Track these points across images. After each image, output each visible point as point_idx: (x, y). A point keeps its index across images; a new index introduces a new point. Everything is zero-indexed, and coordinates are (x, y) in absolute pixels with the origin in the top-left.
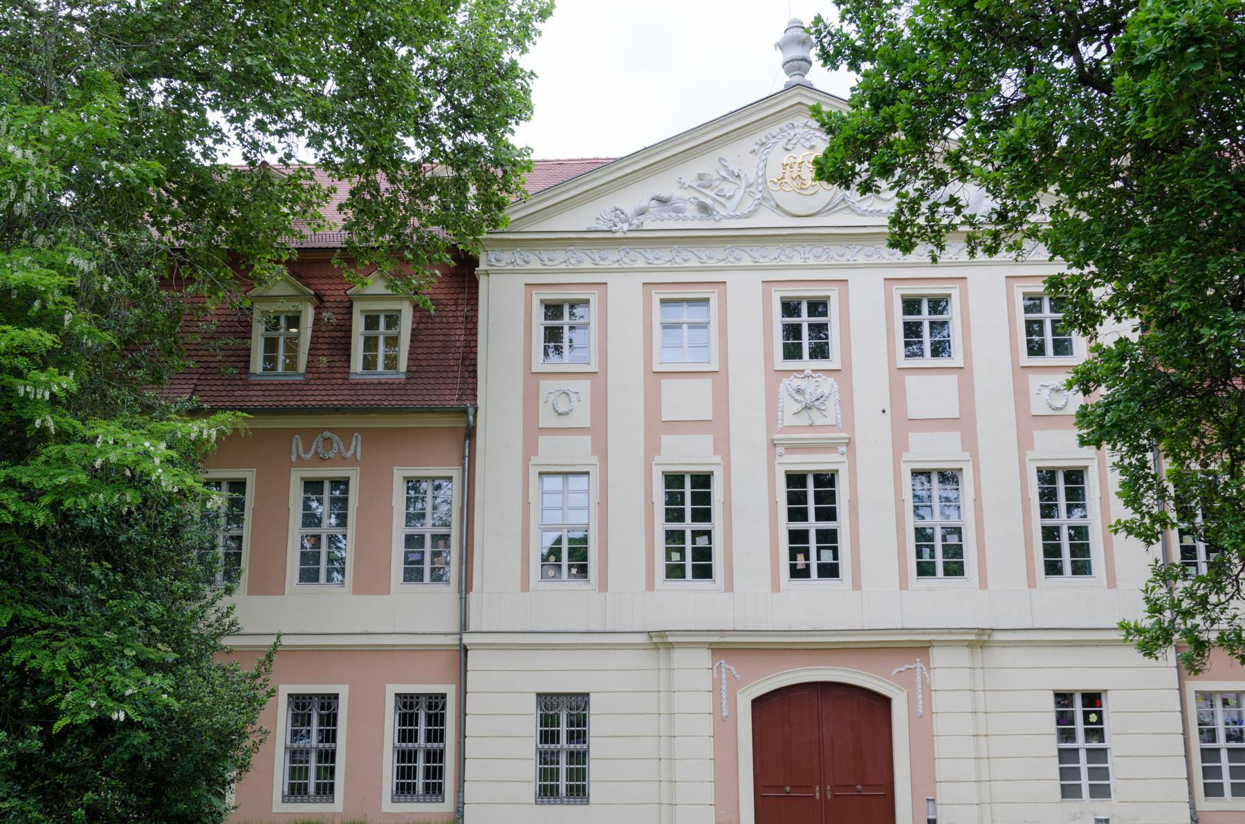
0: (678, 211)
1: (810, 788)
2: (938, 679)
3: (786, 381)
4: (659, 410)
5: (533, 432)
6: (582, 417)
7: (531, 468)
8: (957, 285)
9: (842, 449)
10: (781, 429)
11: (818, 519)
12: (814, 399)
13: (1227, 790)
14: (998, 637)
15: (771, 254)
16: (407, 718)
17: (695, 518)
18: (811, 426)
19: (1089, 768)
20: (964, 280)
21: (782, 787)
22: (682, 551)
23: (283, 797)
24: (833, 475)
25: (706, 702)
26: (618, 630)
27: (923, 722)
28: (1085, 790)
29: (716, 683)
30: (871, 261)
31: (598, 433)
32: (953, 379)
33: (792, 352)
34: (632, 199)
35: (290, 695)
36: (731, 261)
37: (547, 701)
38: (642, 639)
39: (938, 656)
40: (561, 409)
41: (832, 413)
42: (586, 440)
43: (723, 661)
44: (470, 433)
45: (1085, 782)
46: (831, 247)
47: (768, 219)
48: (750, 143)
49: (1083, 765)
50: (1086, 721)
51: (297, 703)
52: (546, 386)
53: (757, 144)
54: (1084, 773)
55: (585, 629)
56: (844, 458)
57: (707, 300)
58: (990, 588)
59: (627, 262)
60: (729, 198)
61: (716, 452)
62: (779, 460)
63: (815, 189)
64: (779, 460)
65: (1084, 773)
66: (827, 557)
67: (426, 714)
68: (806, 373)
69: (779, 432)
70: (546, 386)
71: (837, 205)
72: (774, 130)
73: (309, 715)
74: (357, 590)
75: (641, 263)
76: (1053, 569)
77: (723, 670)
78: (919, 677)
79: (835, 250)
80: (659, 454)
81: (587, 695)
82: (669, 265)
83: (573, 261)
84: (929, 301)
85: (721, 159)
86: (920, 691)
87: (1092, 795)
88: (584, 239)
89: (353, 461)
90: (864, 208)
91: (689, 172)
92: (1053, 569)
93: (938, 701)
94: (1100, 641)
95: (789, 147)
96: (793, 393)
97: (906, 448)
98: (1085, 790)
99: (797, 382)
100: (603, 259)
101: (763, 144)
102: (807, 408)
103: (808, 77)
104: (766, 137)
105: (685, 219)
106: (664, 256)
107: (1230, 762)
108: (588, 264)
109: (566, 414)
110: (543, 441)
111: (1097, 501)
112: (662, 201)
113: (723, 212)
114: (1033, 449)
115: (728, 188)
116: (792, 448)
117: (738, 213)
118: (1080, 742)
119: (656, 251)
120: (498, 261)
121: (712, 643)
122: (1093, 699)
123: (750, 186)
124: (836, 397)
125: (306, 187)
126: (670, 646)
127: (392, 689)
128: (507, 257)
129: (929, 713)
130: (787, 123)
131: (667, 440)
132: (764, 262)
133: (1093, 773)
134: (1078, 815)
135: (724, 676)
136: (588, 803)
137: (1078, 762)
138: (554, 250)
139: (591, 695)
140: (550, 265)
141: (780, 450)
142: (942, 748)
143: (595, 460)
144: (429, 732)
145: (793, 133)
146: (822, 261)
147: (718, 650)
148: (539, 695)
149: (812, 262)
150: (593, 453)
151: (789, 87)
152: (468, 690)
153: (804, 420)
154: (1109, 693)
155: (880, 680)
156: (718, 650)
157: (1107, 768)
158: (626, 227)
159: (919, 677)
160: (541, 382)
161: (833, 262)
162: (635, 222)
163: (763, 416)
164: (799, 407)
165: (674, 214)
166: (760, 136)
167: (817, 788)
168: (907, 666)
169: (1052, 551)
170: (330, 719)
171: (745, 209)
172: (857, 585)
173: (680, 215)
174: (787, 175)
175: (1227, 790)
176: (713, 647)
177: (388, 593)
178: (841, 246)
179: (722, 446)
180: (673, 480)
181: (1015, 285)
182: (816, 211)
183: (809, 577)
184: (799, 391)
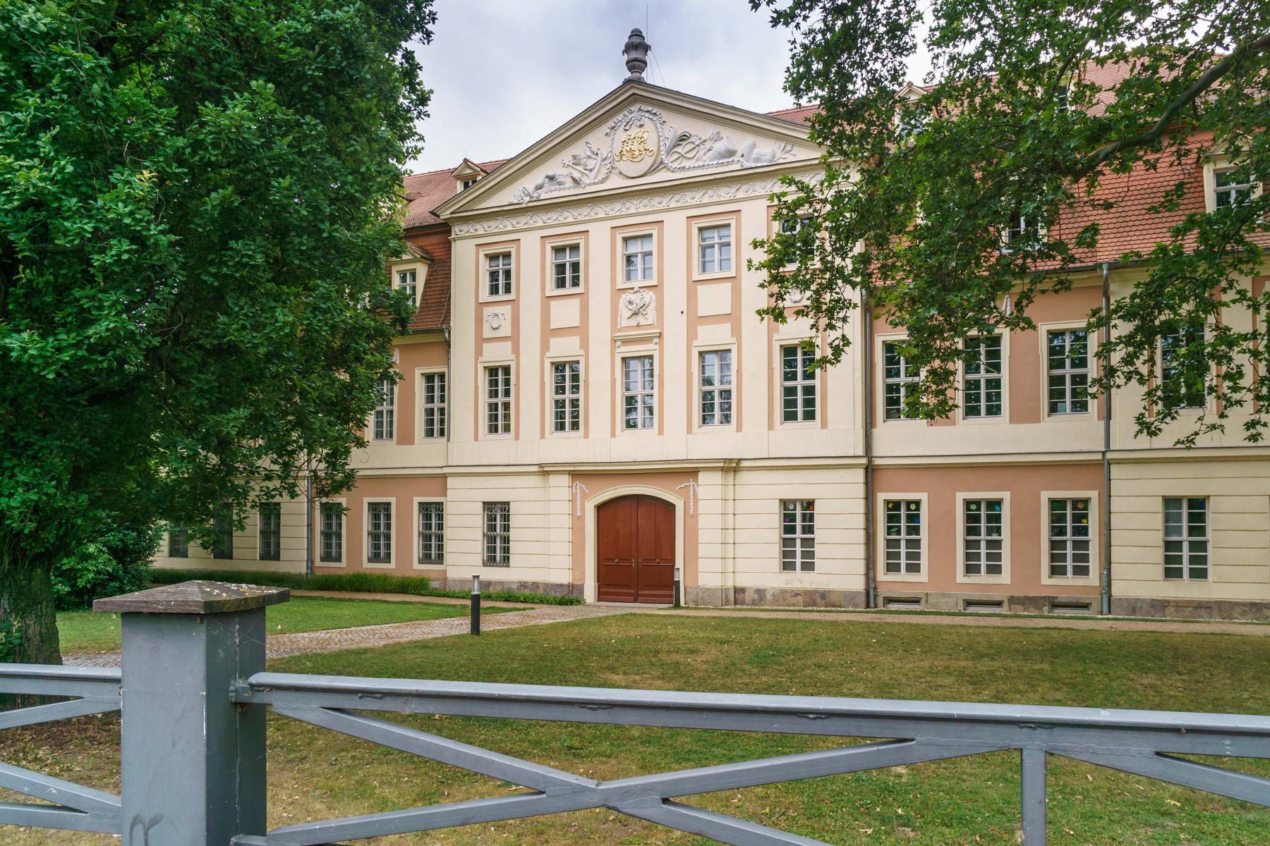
1: (629, 560)
2: (702, 492)
3: (623, 296)
5: (480, 340)
6: (506, 331)
7: (479, 365)
8: (734, 216)
9: (656, 340)
13: (903, 567)
14: (744, 464)
15: (616, 208)
16: (972, 518)
17: (1074, 365)
21: (614, 560)
27: (692, 518)
28: (798, 566)
29: (574, 495)
30: (679, 205)
31: (514, 339)
35: (420, 503)
36: (592, 215)
37: (489, 506)
38: (535, 469)
41: (650, 316)
42: (508, 345)
44: (448, 344)
47: (616, 182)
48: (605, 129)
52: (488, 311)
57: (650, 236)
59: (532, 224)
60: (591, 170)
61: (581, 348)
62: (618, 350)
64: (618, 350)
72: (620, 117)
74: (399, 443)
76: (790, 416)
79: (493, 224)
81: (508, 503)
87: (1075, 573)
92: (790, 416)
93: (702, 507)
97: (696, 337)
98: (798, 566)
102: (636, 314)
103: (643, 75)
106: (553, 217)
109: (497, 328)
110: (486, 346)
112: (551, 178)
115: (591, 164)
116: (626, 342)
118: (799, 535)
123: (605, 159)
124: (653, 305)
126: (548, 473)
127: (417, 500)
128: (465, 228)
131: (554, 342)
133: (804, 555)
141: (619, 343)
144: (804, 527)
147: (576, 475)
148: (484, 503)
151: (627, 82)
153: (633, 322)
156: (576, 475)
158: (527, 199)
162: (535, 195)
163: (609, 320)
164: (630, 313)
166: (611, 123)
169: (789, 403)
170: (914, 518)
180: (559, 367)
184: (630, 303)
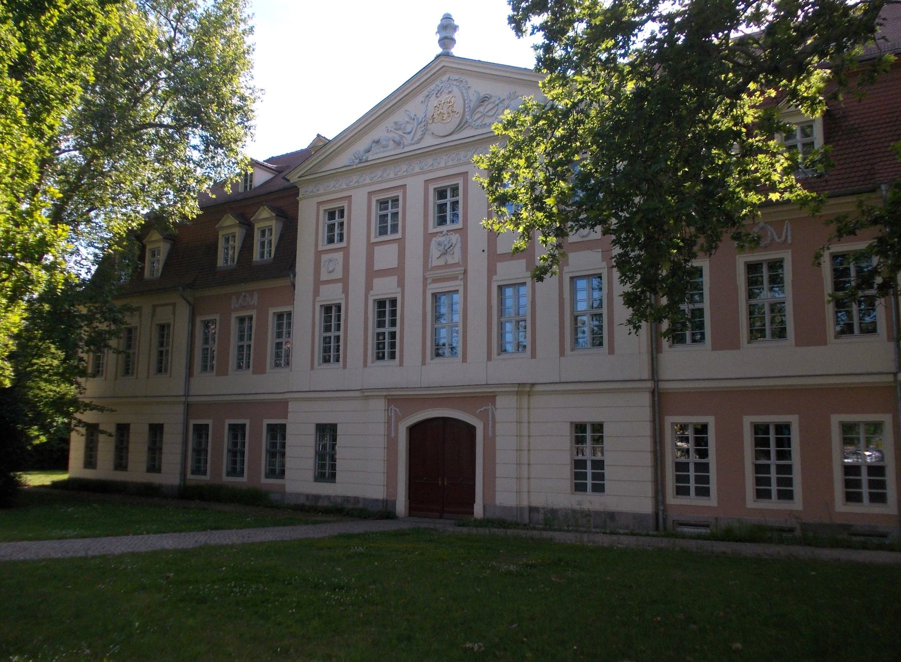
4: (373, 265)
6: (339, 275)
11: (384, 327)
13: (692, 491)
16: (761, 442)
25: (381, 429)
26: (339, 389)
29: (389, 418)
31: (345, 281)
32: (395, 247)
34: (361, 146)
38: (358, 394)
42: (340, 285)
45: (692, 485)
47: (429, 141)
48: (421, 97)
49: (773, 475)
52: (324, 257)
60: (409, 133)
64: (429, 287)
70: (324, 257)
72: (433, 87)
74: (254, 372)
80: (568, 265)
85: (406, 111)
89: (784, 245)
91: (389, 123)
97: (495, 273)
99: (440, 239)
108: (344, 186)
109: (331, 272)
112: (377, 142)
116: (435, 281)
121: (386, 396)
122: (598, 428)
124: (459, 245)
125: (12, 222)
131: (377, 282)
133: (780, 482)
147: (391, 400)
149: (450, 163)
150: (603, 261)
152: (497, 420)
160: (376, 248)
165: (382, 149)
166: (425, 93)
170: (784, 443)
172: (611, 351)
175: (692, 491)
177: (265, 373)
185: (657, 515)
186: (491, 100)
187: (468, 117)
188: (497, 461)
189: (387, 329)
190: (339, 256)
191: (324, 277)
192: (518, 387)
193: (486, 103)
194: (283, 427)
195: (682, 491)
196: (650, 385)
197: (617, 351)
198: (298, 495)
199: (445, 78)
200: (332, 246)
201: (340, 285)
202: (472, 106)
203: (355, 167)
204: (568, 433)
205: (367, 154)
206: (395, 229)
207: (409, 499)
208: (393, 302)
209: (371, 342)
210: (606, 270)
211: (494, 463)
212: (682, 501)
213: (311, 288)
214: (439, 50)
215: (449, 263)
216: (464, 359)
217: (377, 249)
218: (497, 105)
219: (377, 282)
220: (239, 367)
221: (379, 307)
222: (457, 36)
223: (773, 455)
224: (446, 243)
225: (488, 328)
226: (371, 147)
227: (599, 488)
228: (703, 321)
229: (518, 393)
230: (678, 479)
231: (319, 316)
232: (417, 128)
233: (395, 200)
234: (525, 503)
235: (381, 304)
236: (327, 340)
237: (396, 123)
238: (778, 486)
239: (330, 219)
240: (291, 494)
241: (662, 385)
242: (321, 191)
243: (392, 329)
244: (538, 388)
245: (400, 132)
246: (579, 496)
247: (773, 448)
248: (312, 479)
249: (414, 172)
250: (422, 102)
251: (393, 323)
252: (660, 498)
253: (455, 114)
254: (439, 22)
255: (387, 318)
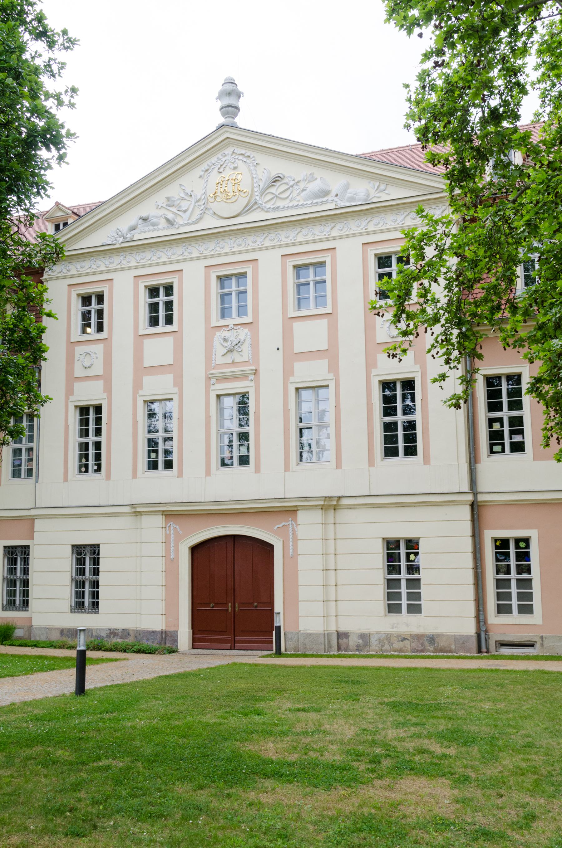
0: (154, 225)
1: (226, 604)
2: (301, 531)
3: (218, 334)
6: (98, 369)
7: (70, 403)
9: (252, 377)
10: (215, 366)
12: (233, 345)
13: (515, 609)
14: (344, 502)
15: (210, 247)
17: (510, 408)
18: (233, 363)
19: (408, 593)
20: (181, 272)
22: (156, 452)
23: (3, 607)
24: (383, 383)
25: (160, 549)
26: (115, 504)
28: (404, 608)
29: (167, 536)
30: (273, 243)
33: (154, 322)
38: (127, 509)
39: (301, 516)
40: (87, 364)
41: (246, 353)
43: (172, 523)
46: (248, 237)
47: (209, 222)
48: (199, 171)
49: (514, 590)
50: (408, 560)
51: (9, 551)
52: (79, 350)
53: (202, 171)
54: (404, 596)
55: (61, 506)
56: (252, 384)
58: (343, 468)
59: (125, 264)
60: (185, 211)
63: (236, 198)
64: (212, 388)
65: (404, 596)
66: (244, 451)
67: (76, 557)
68: (230, 327)
69: (213, 369)
71: (252, 207)
72: (214, 160)
73: (84, 558)
75: (133, 263)
76: (391, 452)
77: (172, 528)
78: (291, 531)
80: (72, 394)
81: (98, 546)
82: (149, 262)
83: (94, 266)
84: (95, 296)
85: (180, 185)
86: (291, 540)
87: (409, 611)
88: (98, 251)
90: (268, 207)
91: (160, 198)
94: (415, 503)
95: (221, 170)
96: (222, 342)
97: (292, 374)
98: (404, 608)
99: (225, 334)
100: (111, 263)
101: (207, 170)
103: (236, 120)
104: (208, 165)
105: (158, 230)
106: (147, 256)
107: (518, 588)
108: (103, 268)
109: (89, 367)
111: (420, 401)
112: (145, 220)
113: (181, 222)
114: (377, 368)
115: (184, 205)
116: (220, 379)
117: (190, 221)
119: (142, 254)
120: (82, 268)
121: (163, 511)
123: (199, 201)
124: (248, 342)
129: (295, 554)
130: (221, 153)
131: (147, 380)
132: (206, 253)
133: (520, 596)
134: (395, 625)
135: (172, 532)
136: (98, 613)
137: (510, 588)
138: (83, 261)
139: (101, 545)
140: (82, 271)
141: (213, 381)
142: (302, 579)
143: (331, 376)
145: (224, 159)
146: (242, 248)
147: (169, 515)
148: (73, 546)
149: (235, 249)
150: (329, 372)
154: (421, 539)
155: (265, 533)
156: (169, 515)
157: (420, 593)
158: (121, 240)
159: (291, 531)
161: (249, 248)
162: (129, 236)
165: (151, 228)
166: (205, 166)
167: (230, 605)
168: (284, 523)
170: (524, 556)
171: (194, 218)
172: (427, 461)
173: (155, 227)
174: (218, 191)
175: (515, 609)
176: (165, 513)
178: (254, 235)
179: (108, 389)
181: (369, 249)
182: (239, 211)
183: (398, 456)
184: (225, 340)
185: (479, 635)
186: (286, 180)
187: (257, 198)
188: (300, 583)
189: (91, 439)
190: (99, 348)
191: (79, 372)
192: (325, 501)
193: (278, 184)
194: (25, 550)
195: (503, 609)
196: (470, 497)
197: (432, 462)
198: (49, 629)
199: (228, 151)
200: (155, 330)
201: (101, 383)
202: (261, 186)
203: (117, 246)
204: (381, 551)
205: (133, 232)
206: (242, 310)
207: (192, 628)
208: (98, 409)
209: (74, 453)
210: (419, 374)
211: (296, 585)
212: (504, 619)
213: (130, 378)
214: (221, 120)
215: (236, 361)
216: (338, 465)
217: (147, 342)
218: (292, 186)
219: (147, 380)
220: (16, 473)
221: (81, 414)
222: (241, 103)
223: (513, 569)
224: (233, 338)
225: (65, 448)
226: (137, 225)
227: (415, 609)
228: (100, 453)
229: (322, 508)
230: (499, 596)
231: (74, 418)
232: (195, 206)
233: (243, 275)
234: (333, 628)
235: (84, 410)
236: (84, 447)
237: (168, 199)
238: (518, 601)
239: (84, 305)
240: (40, 629)
241: (481, 498)
242: (73, 272)
243: (97, 439)
244: (344, 502)
245: (174, 209)
246: (394, 618)
247: (513, 563)
248: (68, 609)
249: (70, 273)
250: (200, 177)
251: (98, 432)
252: (481, 617)
253: (242, 194)
254: (220, 88)
255: (92, 427)
